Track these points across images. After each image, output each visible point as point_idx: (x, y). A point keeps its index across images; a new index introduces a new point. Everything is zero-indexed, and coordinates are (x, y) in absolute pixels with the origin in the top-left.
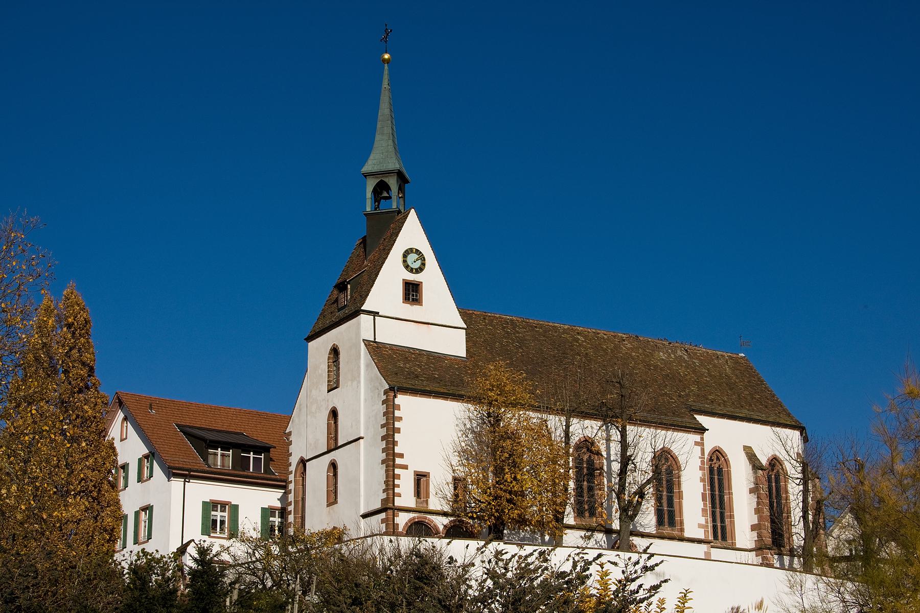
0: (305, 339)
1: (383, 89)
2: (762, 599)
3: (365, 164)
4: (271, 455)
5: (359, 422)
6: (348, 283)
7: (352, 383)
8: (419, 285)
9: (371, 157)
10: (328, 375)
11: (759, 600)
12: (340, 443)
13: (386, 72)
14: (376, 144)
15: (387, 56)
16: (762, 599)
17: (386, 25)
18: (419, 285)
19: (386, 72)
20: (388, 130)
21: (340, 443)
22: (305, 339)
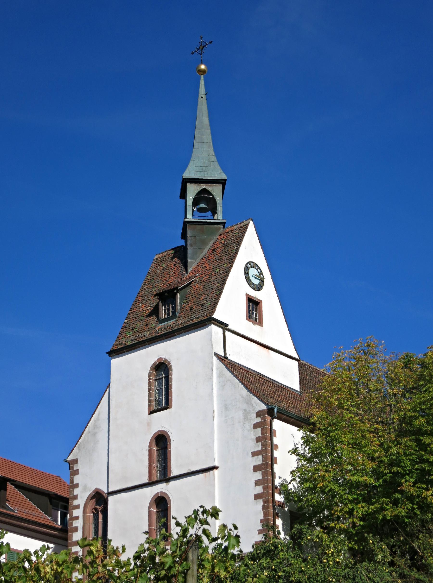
0: (107, 353)
1: (200, 96)
2: (144, 533)
3: (186, 169)
4: (7, 493)
5: (211, 448)
6: (178, 291)
7: (243, 397)
8: (260, 303)
9: (191, 163)
10: (149, 394)
11: (144, 534)
12: (175, 472)
13: (202, 82)
14: (196, 151)
15: (203, 67)
16: (144, 533)
17: (201, 38)
18: (260, 303)
19: (202, 82)
20: (208, 139)
21: (175, 472)
22: (107, 353)
